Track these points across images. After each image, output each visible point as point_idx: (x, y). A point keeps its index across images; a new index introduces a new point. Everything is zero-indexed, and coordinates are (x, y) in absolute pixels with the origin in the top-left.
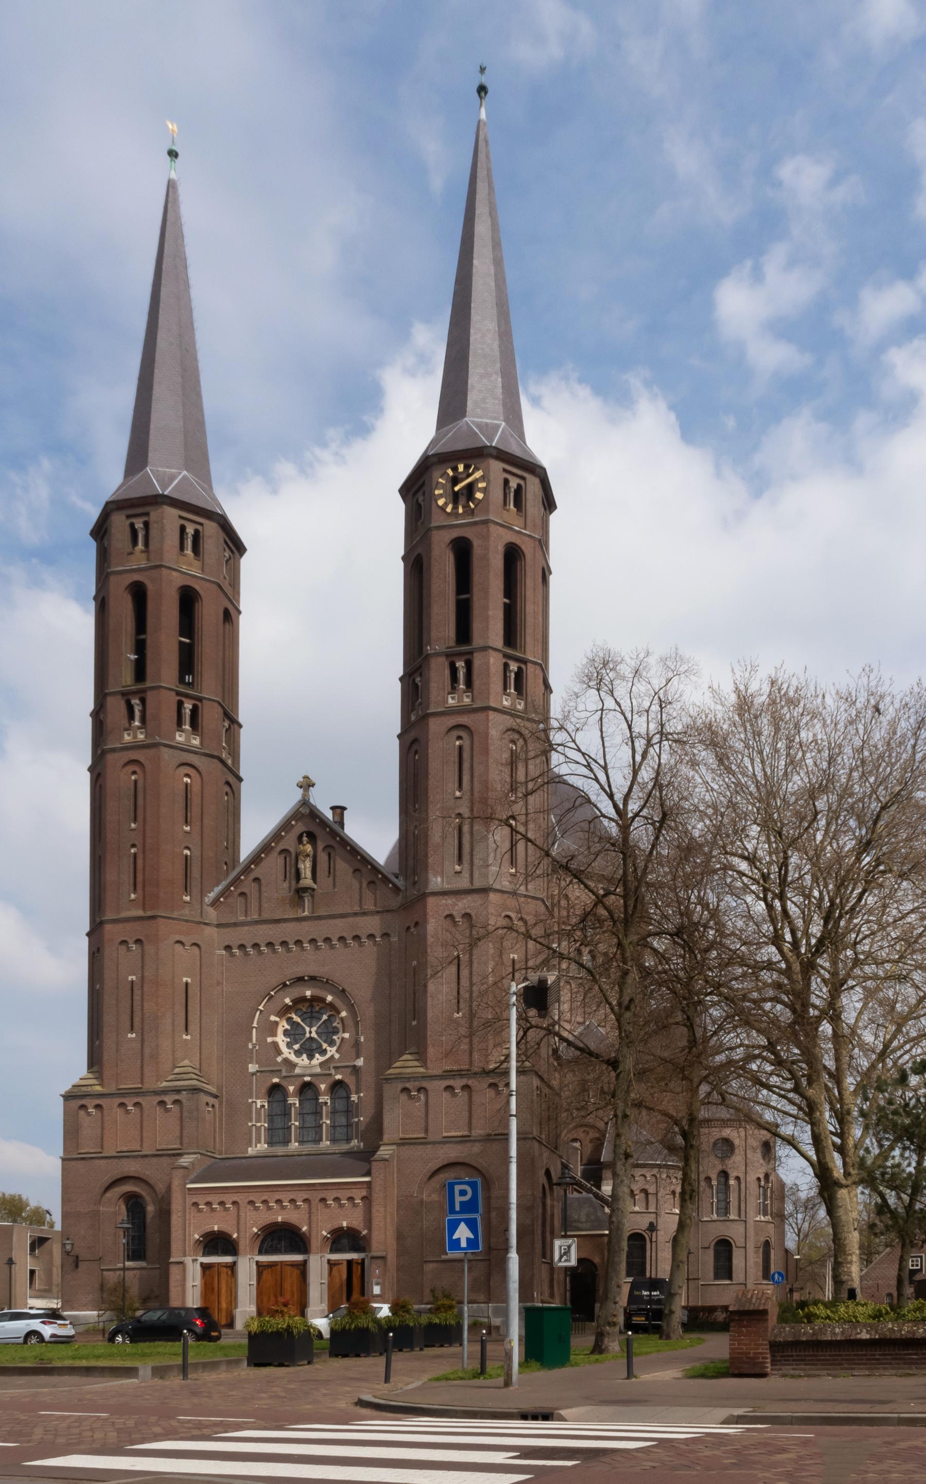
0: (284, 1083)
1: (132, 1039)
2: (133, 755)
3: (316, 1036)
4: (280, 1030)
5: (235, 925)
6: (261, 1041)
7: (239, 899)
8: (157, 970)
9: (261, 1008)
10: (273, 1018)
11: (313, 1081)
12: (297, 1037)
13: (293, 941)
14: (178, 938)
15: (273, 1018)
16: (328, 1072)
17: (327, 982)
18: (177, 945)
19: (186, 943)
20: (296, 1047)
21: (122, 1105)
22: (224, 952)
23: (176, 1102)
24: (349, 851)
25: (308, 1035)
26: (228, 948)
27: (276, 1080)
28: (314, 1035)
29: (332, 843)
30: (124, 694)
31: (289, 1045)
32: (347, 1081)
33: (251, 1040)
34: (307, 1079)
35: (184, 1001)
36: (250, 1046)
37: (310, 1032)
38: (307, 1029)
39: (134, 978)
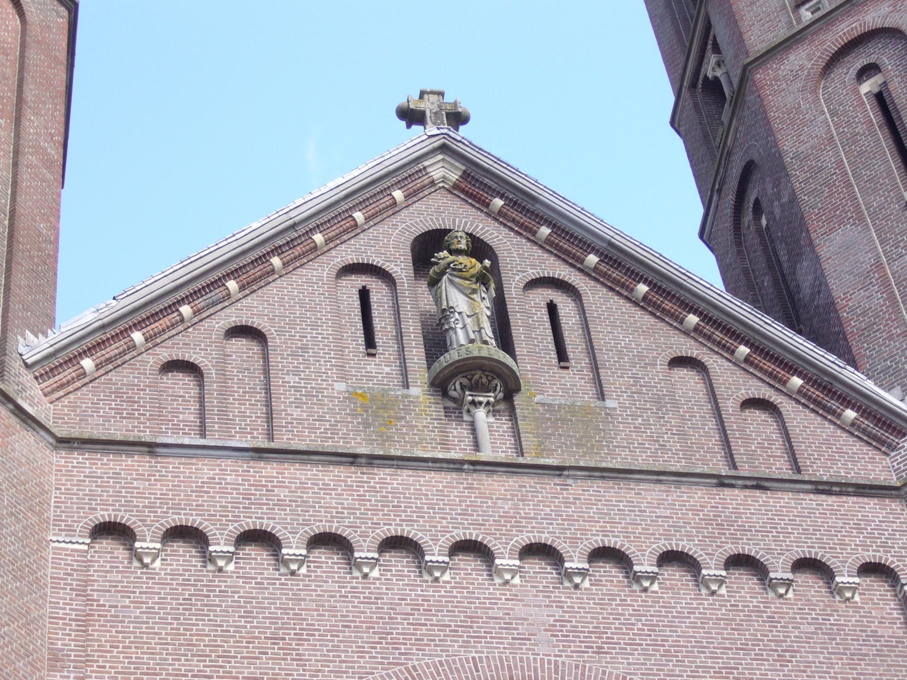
24: (645, 303)
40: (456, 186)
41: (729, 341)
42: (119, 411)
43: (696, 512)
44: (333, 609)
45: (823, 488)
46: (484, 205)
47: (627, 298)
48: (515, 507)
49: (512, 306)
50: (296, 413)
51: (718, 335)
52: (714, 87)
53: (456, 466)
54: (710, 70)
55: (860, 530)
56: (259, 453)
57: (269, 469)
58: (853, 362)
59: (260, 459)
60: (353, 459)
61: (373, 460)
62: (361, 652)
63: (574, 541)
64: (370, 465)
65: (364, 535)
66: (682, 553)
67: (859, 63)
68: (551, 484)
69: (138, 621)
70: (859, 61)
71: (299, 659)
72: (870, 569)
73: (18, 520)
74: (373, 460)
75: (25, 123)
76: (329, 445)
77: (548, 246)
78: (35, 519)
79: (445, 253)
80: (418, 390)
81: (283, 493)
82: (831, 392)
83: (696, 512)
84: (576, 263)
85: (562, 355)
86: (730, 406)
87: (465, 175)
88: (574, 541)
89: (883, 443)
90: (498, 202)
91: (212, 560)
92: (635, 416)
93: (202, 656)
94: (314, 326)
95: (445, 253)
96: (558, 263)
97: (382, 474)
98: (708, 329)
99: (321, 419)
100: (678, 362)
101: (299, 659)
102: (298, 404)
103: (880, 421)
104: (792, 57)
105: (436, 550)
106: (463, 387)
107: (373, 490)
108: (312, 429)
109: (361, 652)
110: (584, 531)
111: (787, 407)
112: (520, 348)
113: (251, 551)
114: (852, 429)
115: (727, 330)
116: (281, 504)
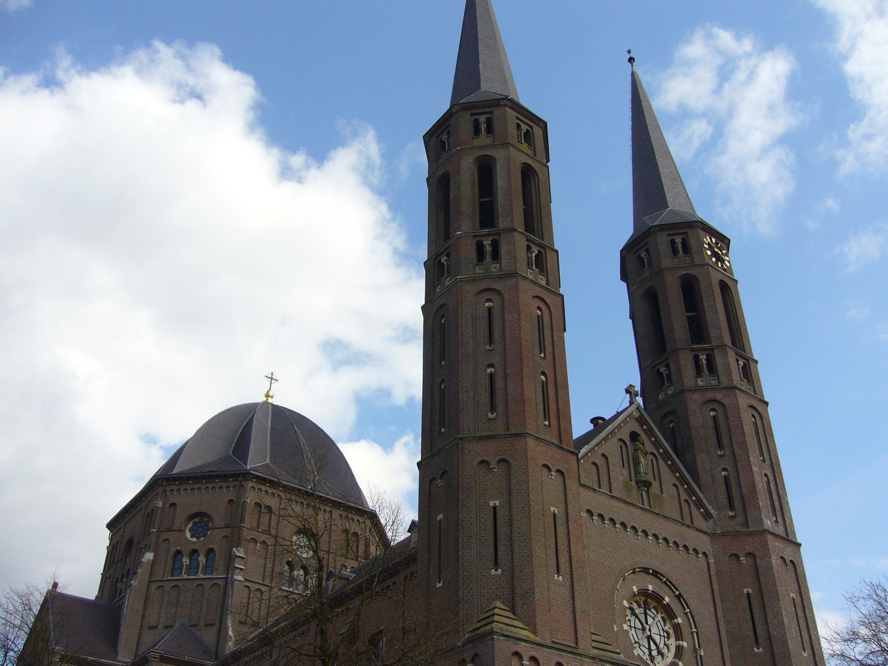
24: (669, 466)
40: (637, 418)
41: (683, 483)
45: (698, 530)
46: (641, 426)
47: (666, 463)
51: (682, 480)
64: (628, 504)
66: (667, 539)
67: (712, 407)
72: (559, 471)
79: (638, 443)
80: (633, 483)
82: (701, 505)
84: (658, 450)
85: (491, 341)
86: (682, 501)
87: (639, 416)
89: (706, 519)
90: (645, 427)
91: (604, 524)
95: (638, 443)
96: (654, 449)
98: (680, 478)
100: (674, 485)
103: (707, 515)
104: (696, 395)
111: (691, 504)
114: (702, 513)
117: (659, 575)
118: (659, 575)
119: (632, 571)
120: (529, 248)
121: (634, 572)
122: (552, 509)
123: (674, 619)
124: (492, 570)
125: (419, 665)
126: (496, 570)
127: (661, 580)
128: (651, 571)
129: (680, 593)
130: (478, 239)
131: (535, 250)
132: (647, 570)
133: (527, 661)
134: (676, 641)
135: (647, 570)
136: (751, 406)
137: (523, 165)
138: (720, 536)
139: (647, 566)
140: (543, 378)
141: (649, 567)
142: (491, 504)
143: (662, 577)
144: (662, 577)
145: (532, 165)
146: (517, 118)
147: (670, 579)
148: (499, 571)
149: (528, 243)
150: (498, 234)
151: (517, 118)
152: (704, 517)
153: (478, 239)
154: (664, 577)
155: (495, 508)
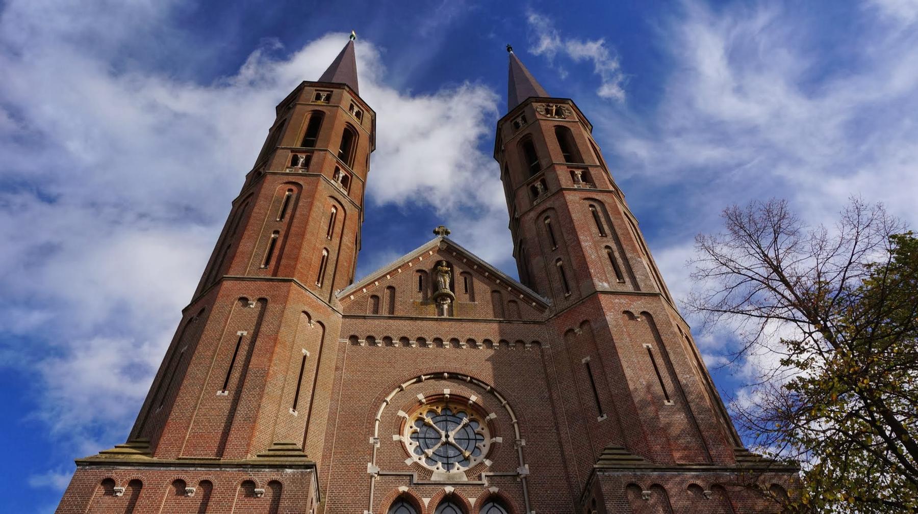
0: (415, 493)
1: (220, 398)
2: (292, 179)
3: (453, 442)
4: (407, 432)
5: (364, 317)
6: (385, 439)
7: (171, 486)
8: (279, 327)
9: (404, 386)
10: (401, 413)
11: (458, 492)
12: (428, 441)
13: (432, 338)
14: (306, 309)
15: (401, 413)
16: (480, 482)
17: (471, 382)
18: (303, 316)
19: (312, 317)
20: (430, 452)
21: (180, 484)
22: (347, 341)
23: (274, 483)
24: (488, 278)
25: (444, 439)
26: (354, 339)
27: (403, 488)
28: (451, 440)
29: (469, 270)
30: (293, 150)
31: (420, 450)
32: (506, 495)
33: (373, 435)
34: (449, 489)
35: (299, 371)
36: (371, 440)
37: (447, 436)
38: (443, 433)
39: (245, 333)
42: (358, 308)
43: (493, 329)
44: (403, 355)
48: (450, 329)
49: (456, 278)
50: (400, 307)
52: (260, 173)
53: (436, 320)
54: (261, 170)
55: (533, 332)
56: (390, 318)
57: (391, 321)
58: (537, 292)
59: (390, 319)
60: (411, 319)
61: (417, 319)
62: (409, 365)
63: (463, 338)
65: (412, 337)
68: (458, 324)
69: (357, 359)
70: (544, 215)
71: (394, 367)
73: (330, 336)
74: (417, 319)
75: (343, 239)
76: (407, 315)
77: (466, 264)
78: (335, 335)
81: (394, 327)
83: (493, 329)
84: (472, 268)
88: (463, 338)
92: (481, 306)
93: (371, 367)
94: (407, 286)
97: (418, 322)
99: (406, 309)
101: (394, 367)
102: (401, 305)
105: (396, 339)
106: (440, 300)
107: (416, 326)
108: (403, 311)
109: (409, 365)
110: (465, 335)
111: (519, 302)
112: (456, 290)
113: (518, 345)
115: (506, 284)
116: (393, 330)
117: (460, 377)
118: (460, 377)
119: (415, 380)
120: (573, 174)
121: (419, 380)
122: (304, 351)
123: (485, 417)
124: (598, 418)
125: (856, 512)
126: (602, 417)
127: (465, 380)
128: (446, 375)
129: (491, 388)
130: (530, 185)
131: (579, 173)
132: (440, 376)
133: (709, 490)
134: (491, 438)
135: (440, 376)
136: (332, 197)
137: (347, 124)
138: (555, 319)
139: (438, 371)
140: (325, 253)
141: (442, 371)
142: (584, 361)
143: (465, 378)
144: (465, 378)
145: (565, 125)
146: (352, 100)
147: (476, 377)
148: (605, 416)
149: (569, 170)
150: (543, 174)
151: (352, 100)
152: (539, 310)
153: (530, 185)
154: (467, 376)
155: (587, 364)
